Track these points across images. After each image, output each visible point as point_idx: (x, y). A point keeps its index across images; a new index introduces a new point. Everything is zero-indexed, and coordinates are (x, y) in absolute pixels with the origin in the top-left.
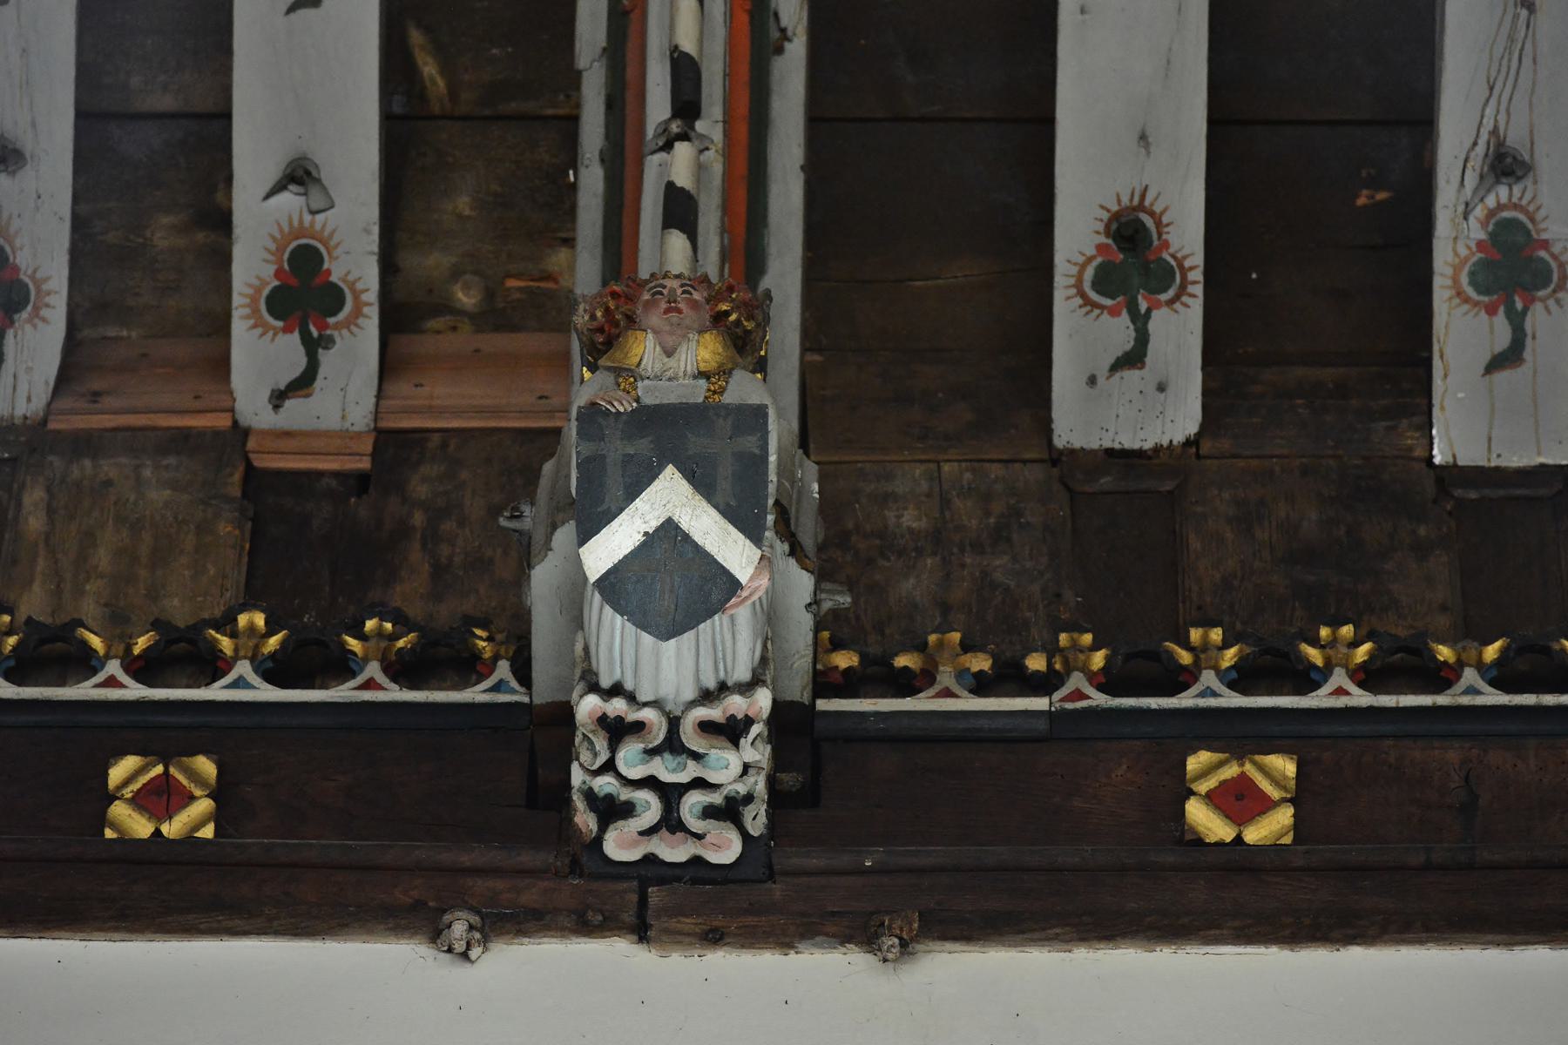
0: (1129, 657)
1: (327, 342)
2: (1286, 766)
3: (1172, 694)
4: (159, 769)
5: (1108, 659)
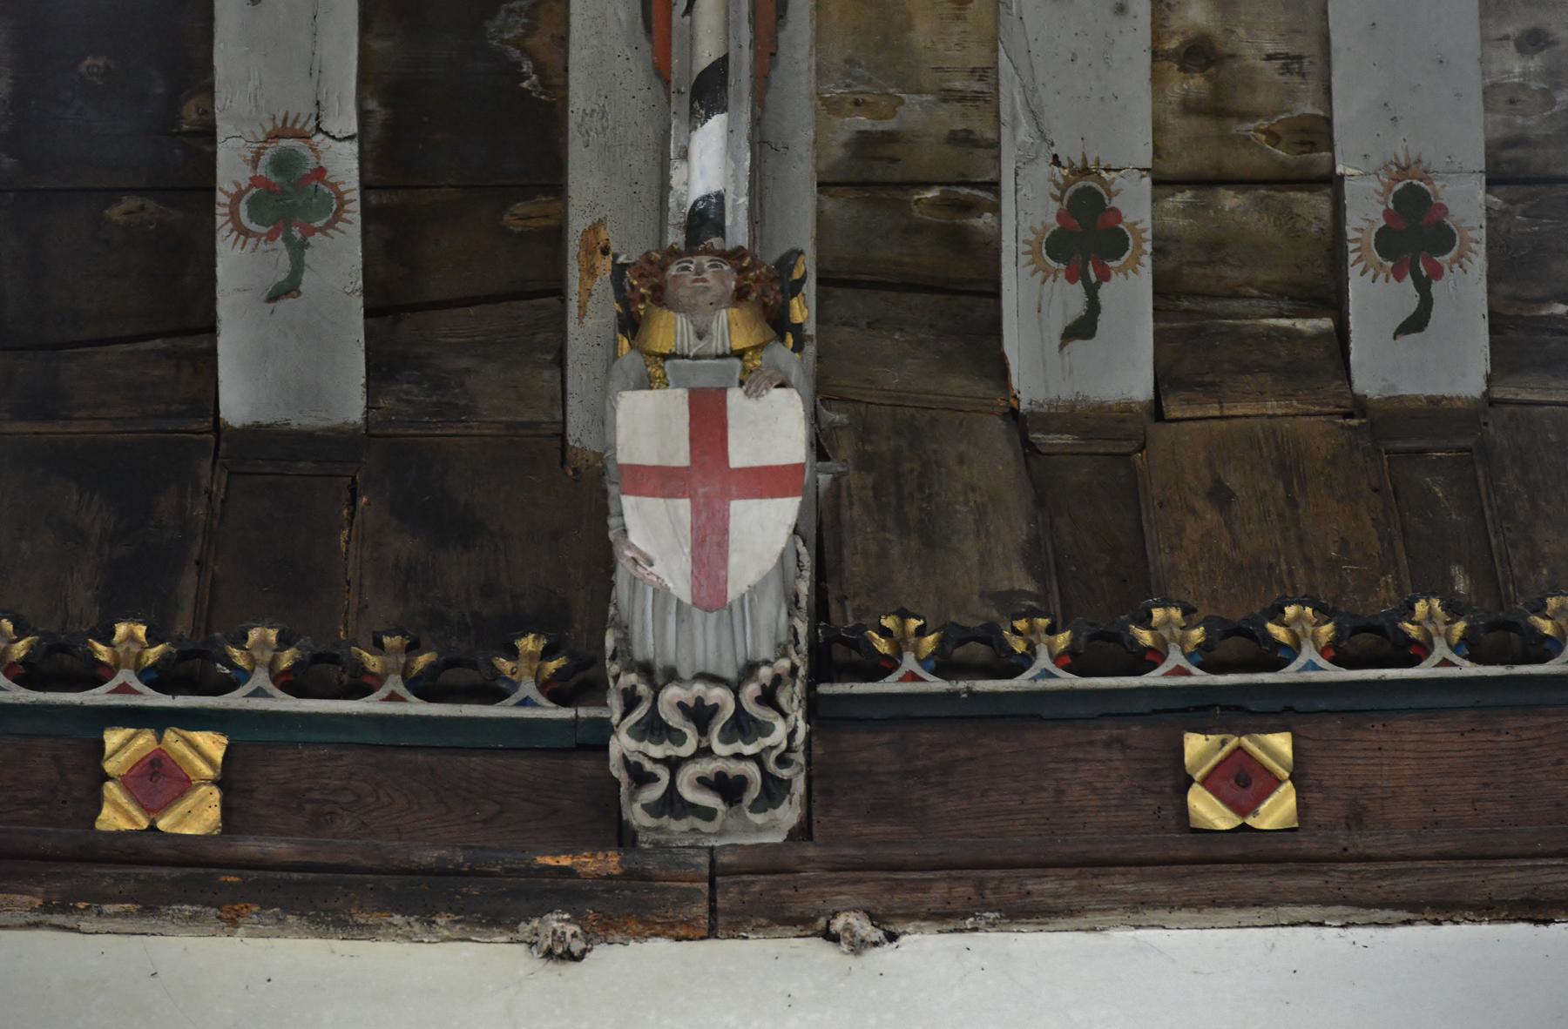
0: (1091, 638)
1: (1437, 273)
2: (1282, 743)
3: (1542, 660)
4: (207, 772)
5: (1073, 641)
